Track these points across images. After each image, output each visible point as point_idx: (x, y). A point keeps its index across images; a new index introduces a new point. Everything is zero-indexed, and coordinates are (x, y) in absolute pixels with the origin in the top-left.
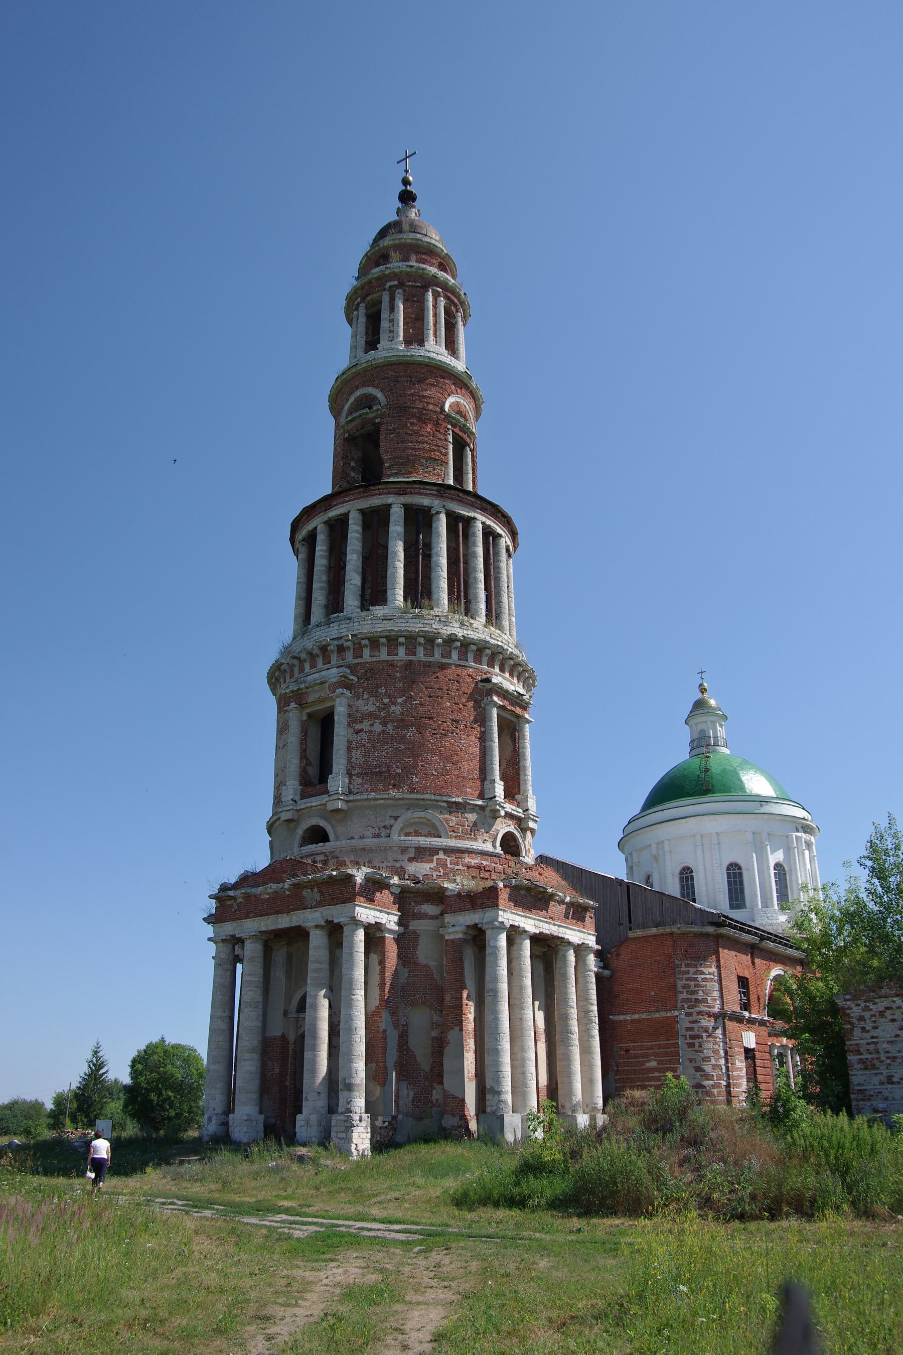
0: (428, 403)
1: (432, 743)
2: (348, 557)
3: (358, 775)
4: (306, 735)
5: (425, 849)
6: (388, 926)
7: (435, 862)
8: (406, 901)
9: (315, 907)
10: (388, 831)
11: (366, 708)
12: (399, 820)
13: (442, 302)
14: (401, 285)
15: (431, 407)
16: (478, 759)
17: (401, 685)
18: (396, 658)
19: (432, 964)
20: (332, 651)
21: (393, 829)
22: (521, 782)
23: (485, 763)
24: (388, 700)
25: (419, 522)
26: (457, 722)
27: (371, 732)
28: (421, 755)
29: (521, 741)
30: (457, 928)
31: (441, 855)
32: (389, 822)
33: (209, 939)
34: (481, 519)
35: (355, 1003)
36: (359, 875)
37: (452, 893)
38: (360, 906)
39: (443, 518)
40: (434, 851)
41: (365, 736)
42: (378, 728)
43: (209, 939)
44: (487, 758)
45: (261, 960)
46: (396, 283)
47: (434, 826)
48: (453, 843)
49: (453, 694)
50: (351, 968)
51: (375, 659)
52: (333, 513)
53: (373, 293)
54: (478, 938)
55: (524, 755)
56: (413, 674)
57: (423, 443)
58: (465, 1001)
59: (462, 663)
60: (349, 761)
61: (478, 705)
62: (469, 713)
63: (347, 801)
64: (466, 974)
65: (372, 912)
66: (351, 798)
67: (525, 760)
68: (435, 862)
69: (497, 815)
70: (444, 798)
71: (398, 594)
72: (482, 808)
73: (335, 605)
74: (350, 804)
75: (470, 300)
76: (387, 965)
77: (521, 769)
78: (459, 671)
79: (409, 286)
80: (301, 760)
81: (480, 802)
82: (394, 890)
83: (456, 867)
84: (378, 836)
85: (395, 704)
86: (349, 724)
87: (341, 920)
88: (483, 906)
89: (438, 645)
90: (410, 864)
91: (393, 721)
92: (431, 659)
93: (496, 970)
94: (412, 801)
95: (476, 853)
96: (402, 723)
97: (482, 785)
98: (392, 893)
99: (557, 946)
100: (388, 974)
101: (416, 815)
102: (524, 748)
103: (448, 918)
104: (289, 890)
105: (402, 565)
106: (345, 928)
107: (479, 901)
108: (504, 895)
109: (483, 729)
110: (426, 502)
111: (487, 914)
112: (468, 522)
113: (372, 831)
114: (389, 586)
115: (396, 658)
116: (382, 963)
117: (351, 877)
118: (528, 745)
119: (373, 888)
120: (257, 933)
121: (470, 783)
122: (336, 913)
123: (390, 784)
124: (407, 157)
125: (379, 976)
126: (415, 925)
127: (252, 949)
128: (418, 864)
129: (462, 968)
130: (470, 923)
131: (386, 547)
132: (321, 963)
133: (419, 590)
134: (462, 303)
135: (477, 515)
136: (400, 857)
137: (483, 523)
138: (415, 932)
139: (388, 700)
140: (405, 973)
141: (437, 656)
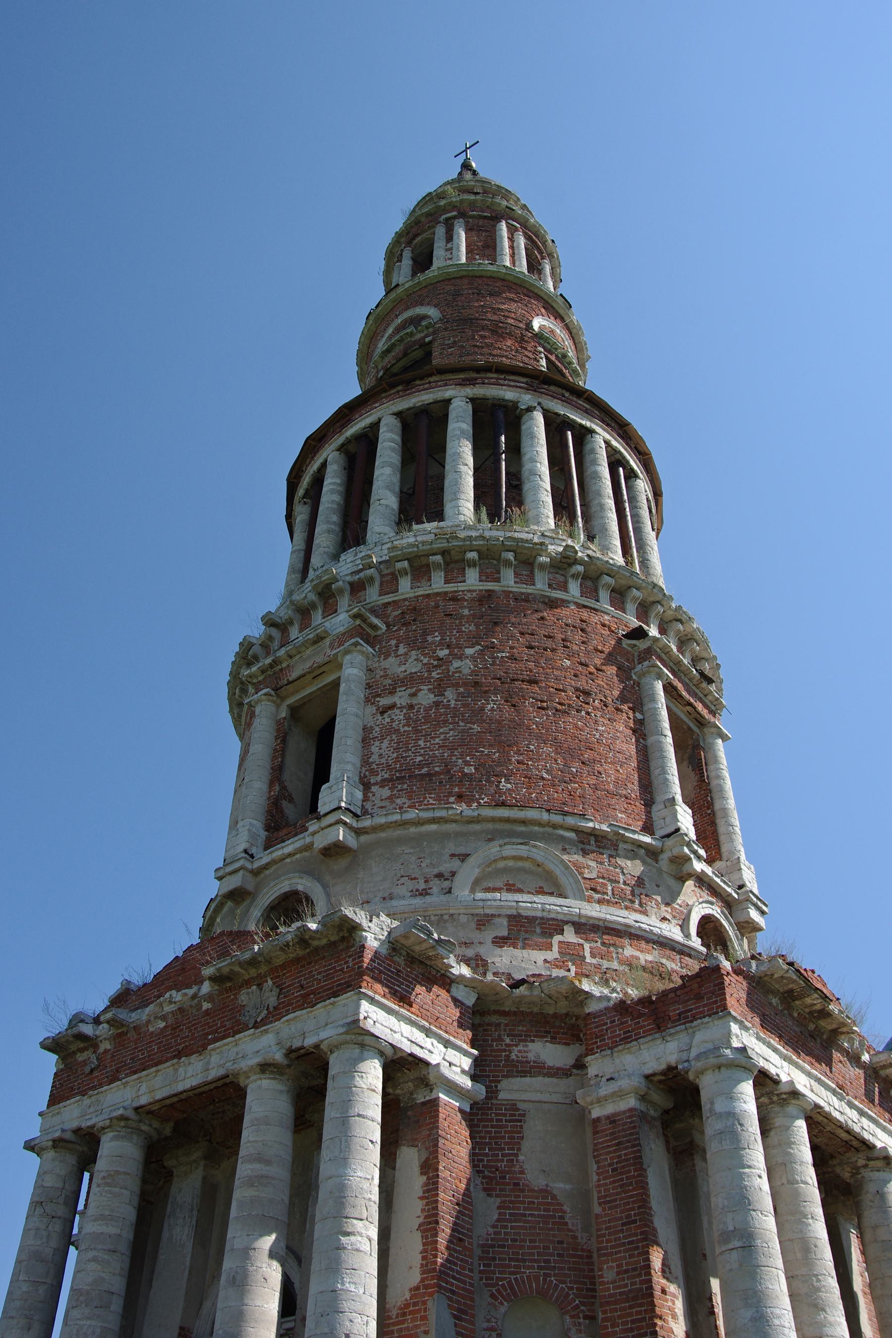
0: (506, 317)
1: (537, 724)
2: (377, 473)
3: (383, 784)
4: (284, 741)
5: (532, 920)
6: (445, 1070)
7: (555, 948)
8: (489, 1021)
9: (264, 1022)
10: (446, 884)
11: (403, 668)
12: (471, 860)
13: (521, 241)
14: (462, 215)
15: (510, 321)
16: (634, 764)
17: (472, 628)
18: (461, 587)
19: (560, 1187)
20: (341, 591)
21: (457, 878)
22: (722, 838)
23: (649, 775)
24: (447, 652)
25: (496, 428)
26: (587, 693)
27: (411, 707)
28: (516, 743)
29: (711, 767)
30: (623, 1083)
31: (570, 936)
32: (446, 867)
33: (30, 1146)
34: (602, 437)
35: (350, 1260)
36: (375, 933)
37: (603, 1005)
38: (372, 1001)
39: (539, 418)
40: (551, 926)
41: (398, 715)
42: (426, 698)
43: (30, 1146)
44: (653, 765)
45: (134, 1184)
46: (455, 213)
47: (550, 877)
48: (594, 911)
49: (575, 648)
50: (343, 1160)
51: (420, 592)
52: (352, 430)
53: (426, 231)
54: (679, 1103)
55: (721, 790)
56: (492, 610)
57: (502, 356)
58: (659, 1280)
59: (591, 603)
60: (366, 761)
61: (624, 673)
62: (609, 682)
63: (358, 832)
64: (654, 1204)
65: (406, 1029)
66: (367, 823)
67: (724, 798)
68: (555, 948)
69: (686, 869)
70: (570, 821)
71: (464, 504)
72: (652, 853)
73: (353, 531)
74: (363, 838)
75: (561, 251)
76: (443, 1173)
77: (719, 814)
78: (585, 614)
79: (472, 217)
80: (271, 783)
81: (647, 839)
82: (460, 992)
83: (605, 964)
84: (425, 893)
85: (461, 658)
86: (367, 700)
87: (323, 1035)
88: (686, 1018)
89: (542, 566)
90: (498, 951)
91: (457, 685)
92: (529, 590)
93: (741, 1177)
94: (499, 826)
95: (648, 941)
96: (475, 687)
97: (648, 813)
98: (455, 1001)
99: (856, 1171)
100: (446, 1200)
101: (509, 851)
102: (719, 777)
103: (596, 1065)
104: (209, 998)
105: (471, 473)
106: (333, 1059)
107: (674, 1010)
108: (736, 992)
109: (639, 716)
110: (509, 395)
111: (699, 1037)
112: (583, 435)
113: (411, 885)
114: (447, 497)
115: (461, 587)
116: (430, 1167)
117: (353, 928)
118: (726, 774)
119: (409, 971)
120: (130, 1113)
121: (622, 804)
122: (312, 1026)
123: (450, 794)
124: (467, 148)
125: (420, 1205)
126: (513, 1089)
127: (118, 1154)
128: (518, 953)
129: (643, 1186)
130: (653, 1066)
131: (442, 448)
132: (268, 1162)
133: (500, 492)
134: (551, 255)
135: (598, 429)
136: (476, 936)
137: (607, 443)
138: (513, 1106)
139: (447, 652)
140: (489, 1210)
141: (541, 584)
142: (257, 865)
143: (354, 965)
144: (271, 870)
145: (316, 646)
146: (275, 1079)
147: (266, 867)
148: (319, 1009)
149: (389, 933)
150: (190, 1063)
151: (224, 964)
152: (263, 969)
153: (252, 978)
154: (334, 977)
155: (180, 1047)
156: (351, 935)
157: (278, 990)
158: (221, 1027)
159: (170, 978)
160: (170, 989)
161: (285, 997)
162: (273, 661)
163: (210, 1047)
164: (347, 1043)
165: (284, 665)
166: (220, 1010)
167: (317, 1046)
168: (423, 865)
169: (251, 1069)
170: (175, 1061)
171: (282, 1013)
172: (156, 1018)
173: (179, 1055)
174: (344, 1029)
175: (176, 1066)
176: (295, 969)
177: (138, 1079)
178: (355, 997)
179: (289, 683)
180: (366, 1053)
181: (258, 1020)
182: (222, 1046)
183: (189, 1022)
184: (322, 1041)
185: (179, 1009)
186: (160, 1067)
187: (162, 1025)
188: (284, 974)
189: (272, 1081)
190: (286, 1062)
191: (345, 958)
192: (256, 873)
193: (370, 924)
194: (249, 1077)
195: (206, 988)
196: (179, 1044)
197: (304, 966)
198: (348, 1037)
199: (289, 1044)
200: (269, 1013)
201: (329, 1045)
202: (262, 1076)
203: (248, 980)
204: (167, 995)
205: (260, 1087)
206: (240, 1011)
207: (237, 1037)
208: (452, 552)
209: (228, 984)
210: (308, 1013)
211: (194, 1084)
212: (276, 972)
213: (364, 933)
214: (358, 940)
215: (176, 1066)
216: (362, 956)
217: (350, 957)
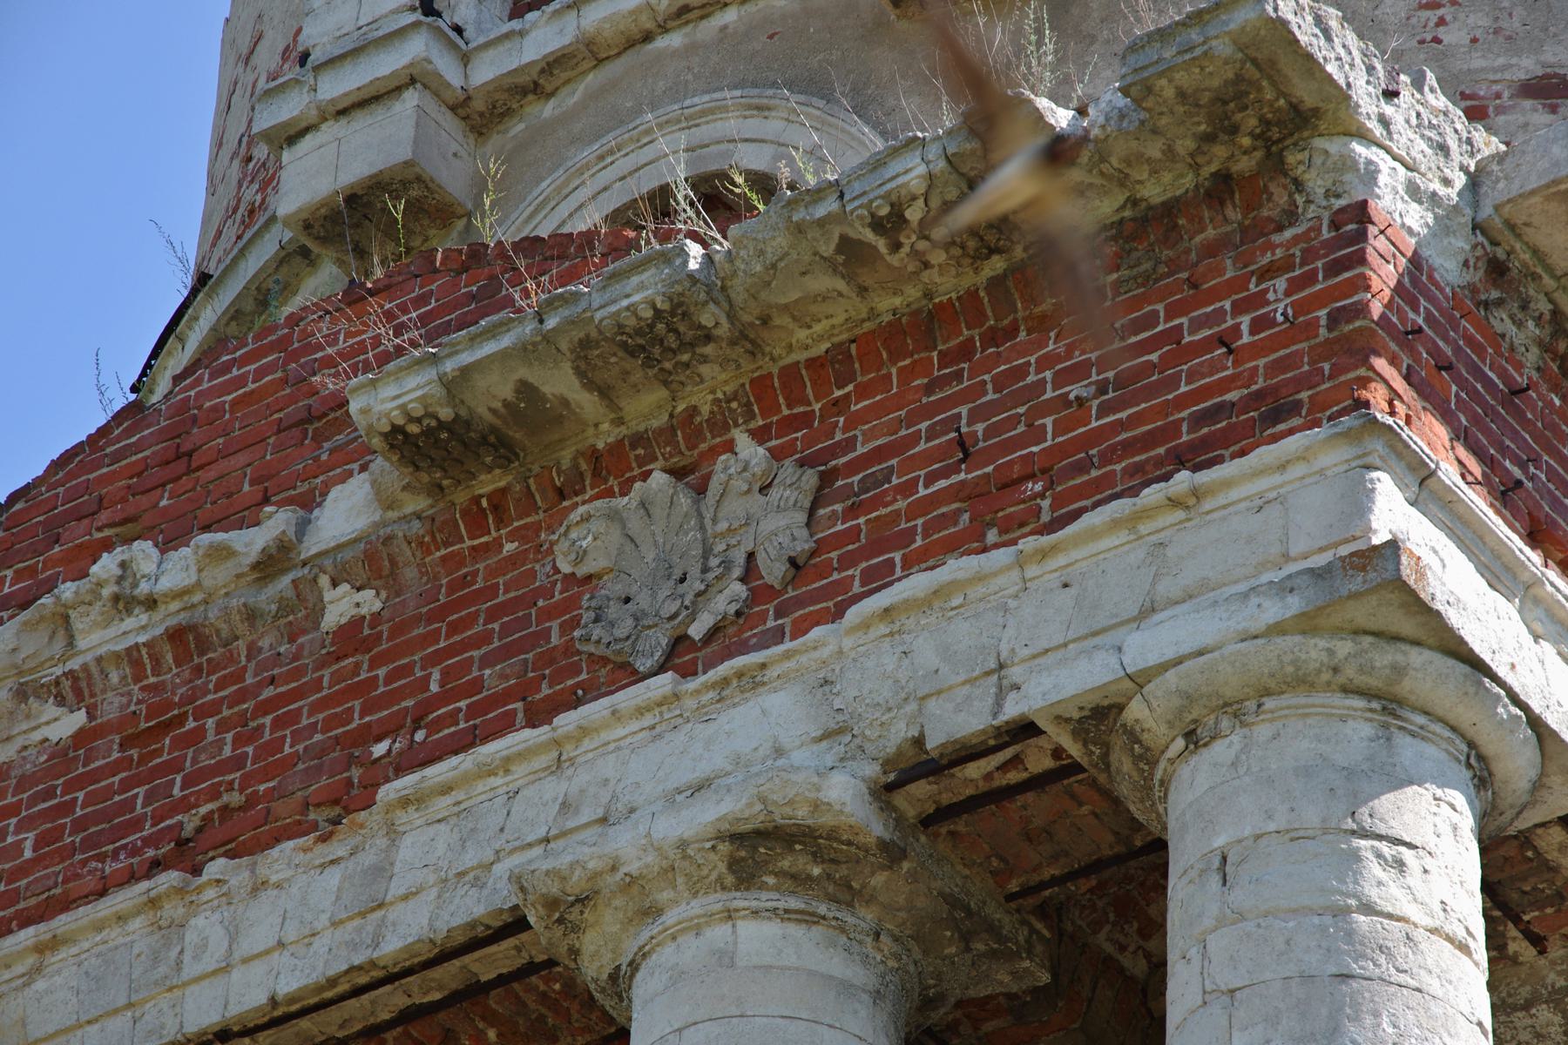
9: (726, 639)
38: (1422, 485)
87: (1145, 647)
104: (370, 561)
142: (486, 71)
143: (1301, 308)
144: (571, 97)
146: (809, 918)
147: (534, 84)
148: (1093, 534)
149: (1475, 182)
150: (259, 887)
151: (489, 348)
152: (712, 383)
153: (638, 440)
154: (1174, 382)
155: (190, 822)
156: (1275, 163)
157: (810, 478)
158: (446, 697)
159: (101, 504)
160: (131, 528)
161: (852, 512)
163: (388, 792)
164: (1301, 681)
166: (440, 614)
167: (1100, 717)
168: (1449, 36)
169: (678, 864)
170: (170, 878)
171: (845, 584)
173: (187, 855)
174: (1295, 604)
175: (172, 910)
176: (906, 375)
178: (1335, 458)
180: (1408, 749)
181: (696, 631)
182: (467, 779)
183: (241, 696)
184: (1139, 680)
185: (176, 635)
186: (62, 923)
187: (65, 724)
188: (839, 405)
189: (795, 931)
190: (878, 829)
191: (1240, 283)
192: (482, 115)
193: (1389, 110)
194: (652, 912)
195: (347, 512)
196: (184, 805)
197: (966, 351)
198: (1314, 650)
199: (900, 732)
200: (760, 593)
201: (1189, 698)
202: (740, 901)
203: (617, 448)
204: (106, 566)
205: (726, 958)
206: (571, 603)
207: (567, 721)
209: (488, 483)
210: (1021, 562)
211: (287, 985)
212: (786, 404)
213: (1358, 148)
214: (1317, 184)
215: (172, 910)
216: (1361, 259)
217: (1267, 273)
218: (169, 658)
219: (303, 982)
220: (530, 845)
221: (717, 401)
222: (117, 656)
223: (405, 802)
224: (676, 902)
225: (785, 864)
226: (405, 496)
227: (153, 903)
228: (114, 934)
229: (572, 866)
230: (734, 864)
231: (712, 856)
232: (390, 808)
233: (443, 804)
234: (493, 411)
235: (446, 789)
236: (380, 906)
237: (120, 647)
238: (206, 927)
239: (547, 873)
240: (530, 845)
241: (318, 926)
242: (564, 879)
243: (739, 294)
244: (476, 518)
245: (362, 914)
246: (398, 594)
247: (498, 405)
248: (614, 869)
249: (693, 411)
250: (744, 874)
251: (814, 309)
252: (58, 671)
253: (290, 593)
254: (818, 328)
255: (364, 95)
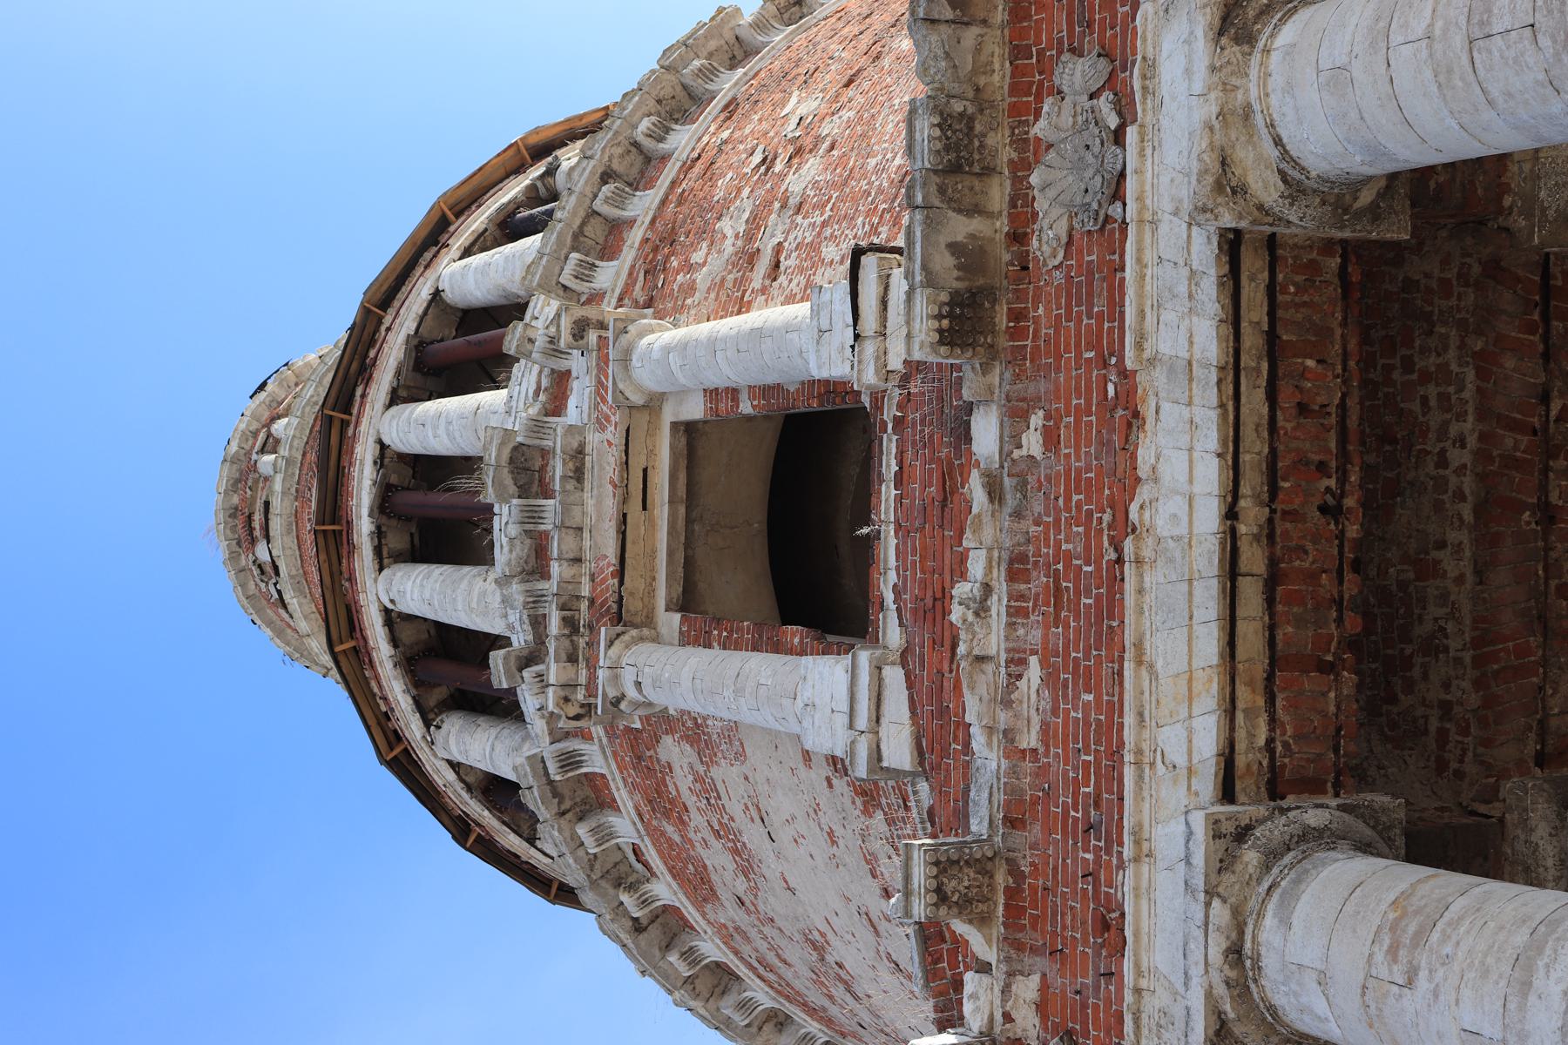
145: (587, 475)
162: (562, 608)
165: (585, 591)
169: (1225, 78)
172: (1007, 703)
173: (1123, 527)
177: (1138, 764)
179: (621, 573)
182: (1140, 295)
185: (1013, 576)
194: (1247, 113)
202: (1261, 44)
208: (615, 166)
218: (1023, 587)
219: (1215, 427)
220: (1189, 236)
221: (1011, 144)
222: (1011, 626)
223: (1139, 346)
224: (1247, 90)
225: (1251, 13)
226: (989, 378)
227: (1139, 561)
228: (1148, 599)
229: (1200, 160)
230: (1237, 40)
231: (1226, 52)
232: (1138, 358)
233: (1150, 318)
234: (957, 279)
235: (1141, 314)
236: (1190, 363)
237: (1004, 619)
238: (1163, 526)
239: (1199, 181)
240: (1189, 236)
241: (1187, 416)
242: (1206, 171)
243: (955, 88)
244: (1016, 333)
245: (1191, 380)
246: (1040, 399)
247: (956, 273)
248: (1211, 129)
249: (1011, 161)
250: (1246, 38)
251: (983, 58)
252: (1003, 670)
253: (1015, 480)
254: (997, 66)
255: (874, 700)
